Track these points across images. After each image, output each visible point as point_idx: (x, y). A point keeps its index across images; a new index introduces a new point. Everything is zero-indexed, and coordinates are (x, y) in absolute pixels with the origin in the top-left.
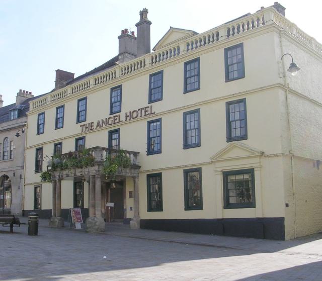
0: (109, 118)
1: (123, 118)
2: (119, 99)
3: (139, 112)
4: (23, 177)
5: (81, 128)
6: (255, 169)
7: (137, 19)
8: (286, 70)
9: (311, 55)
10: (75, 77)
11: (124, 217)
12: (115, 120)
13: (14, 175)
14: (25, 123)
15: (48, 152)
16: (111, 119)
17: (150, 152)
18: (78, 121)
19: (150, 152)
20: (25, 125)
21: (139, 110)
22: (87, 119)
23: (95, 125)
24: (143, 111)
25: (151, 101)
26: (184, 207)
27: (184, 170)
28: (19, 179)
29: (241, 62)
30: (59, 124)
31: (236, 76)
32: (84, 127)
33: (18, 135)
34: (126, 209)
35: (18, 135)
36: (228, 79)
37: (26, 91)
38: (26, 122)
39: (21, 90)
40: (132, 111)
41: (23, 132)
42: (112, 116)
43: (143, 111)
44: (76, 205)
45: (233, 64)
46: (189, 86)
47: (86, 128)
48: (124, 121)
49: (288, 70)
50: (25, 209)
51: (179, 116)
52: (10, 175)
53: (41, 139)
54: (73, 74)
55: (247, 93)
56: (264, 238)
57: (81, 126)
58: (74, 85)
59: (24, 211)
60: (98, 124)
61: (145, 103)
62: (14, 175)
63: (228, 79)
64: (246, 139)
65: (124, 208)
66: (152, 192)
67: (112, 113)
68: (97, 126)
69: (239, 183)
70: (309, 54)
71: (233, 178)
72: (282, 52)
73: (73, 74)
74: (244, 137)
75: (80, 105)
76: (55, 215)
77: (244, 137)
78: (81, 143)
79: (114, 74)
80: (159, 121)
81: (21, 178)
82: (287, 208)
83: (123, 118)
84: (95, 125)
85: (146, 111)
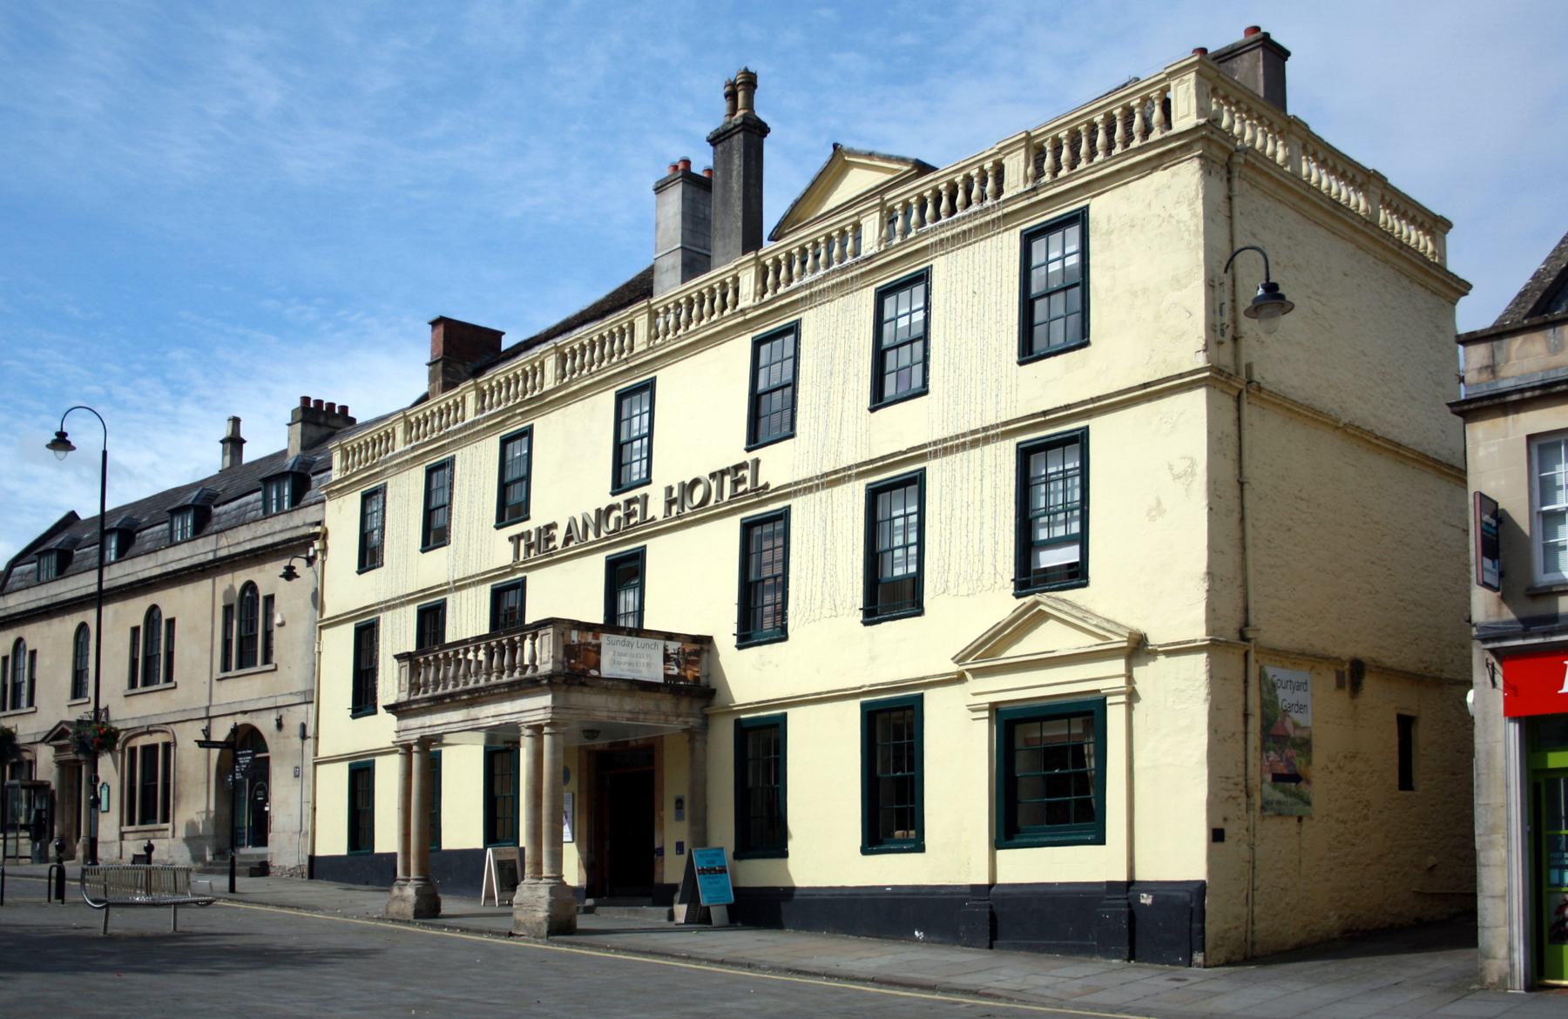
0: (611, 508)
1: (656, 509)
2: (788, 377)
3: (714, 485)
4: (310, 731)
5: (511, 546)
6: (1109, 700)
7: (717, 115)
8: (1241, 309)
9: (1360, 247)
10: (506, 343)
11: (657, 880)
12: (629, 516)
13: (280, 725)
14: (318, 529)
15: (399, 633)
16: (616, 514)
17: (747, 635)
18: (501, 522)
19: (747, 635)
20: (316, 536)
21: (713, 475)
22: (653, 477)
23: (560, 534)
24: (727, 480)
25: (754, 442)
26: (859, 843)
27: (863, 705)
28: (298, 740)
29: (444, 506)
30: (435, 535)
31: (1058, 339)
32: (522, 543)
33: (290, 574)
34: (661, 851)
35: (290, 574)
36: (1028, 352)
37: (326, 400)
38: (318, 523)
39: (306, 400)
40: (603, 508)
41: (310, 561)
42: (620, 499)
43: (727, 480)
44: (491, 836)
45: (631, 442)
46: (890, 381)
47: (529, 547)
48: (660, 518)
49: (1247, 313)
50: (319, 852)
51: (853, 497)
52: (265, 724)
53: (435, 568)
54: (498, 335)
55: (921, 453)
56: (1132, 956)
57: (511, 539)
58: (499, 373)
59: (312, 859)
60: (569, 530)
61: (735, 452)
62: (280, 725)
63: (1028, 352)
64: (1085, 585)
65: (657, 845)
66: (750, 784)
67: (618, 486)
68: (567, 540)
69: (1054, 755)
70: (1353, 241)
71: (1033, 732)
72: (1232, 241)
73: (498, 335)
74: (1076, 575)
75: (763, 361)
76: (407, 870)
77: (1076, 575)
78: (511, 604)
79: (460, 409)
80: (781, 519)
81: (304, 737)
82: (1219, 845)
83: (656, 509)
84: (560, 534)
85: (736, 483)
